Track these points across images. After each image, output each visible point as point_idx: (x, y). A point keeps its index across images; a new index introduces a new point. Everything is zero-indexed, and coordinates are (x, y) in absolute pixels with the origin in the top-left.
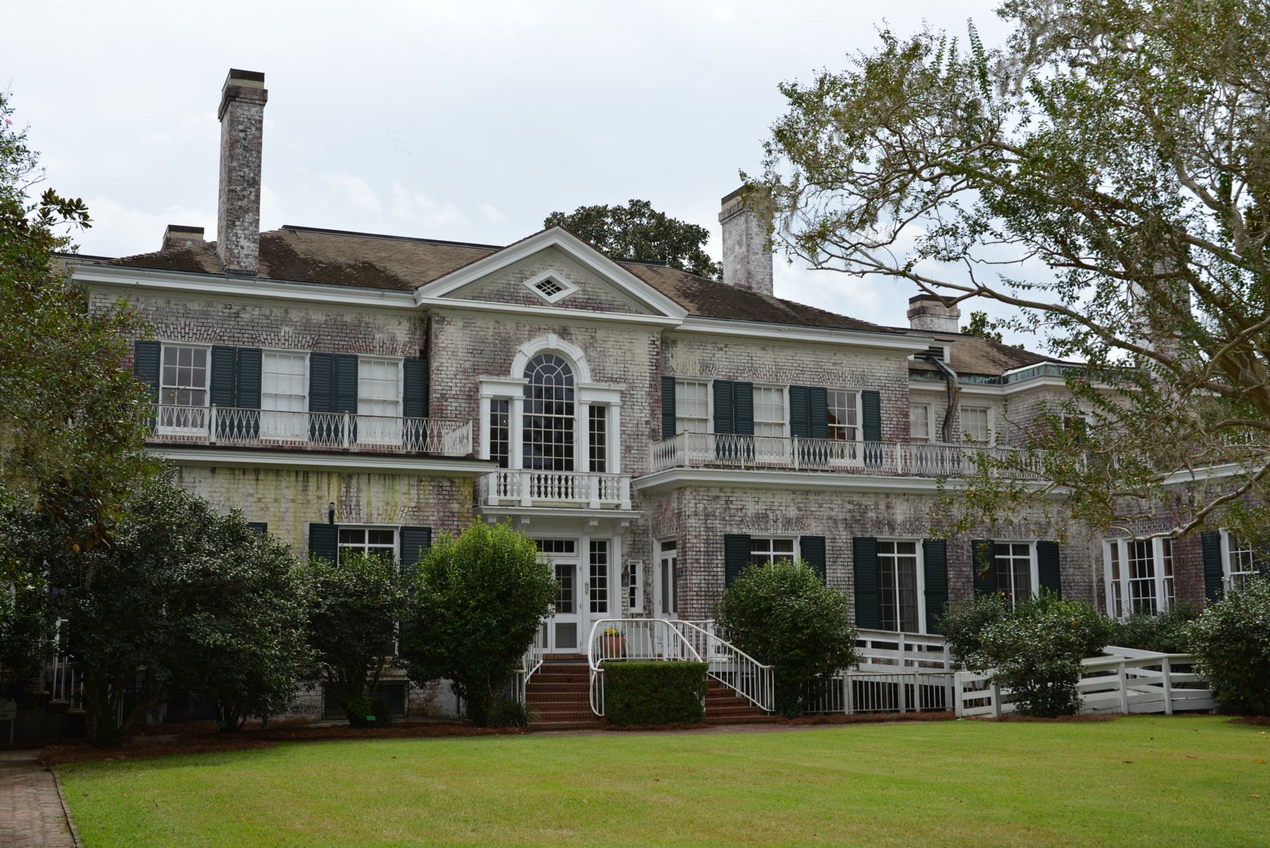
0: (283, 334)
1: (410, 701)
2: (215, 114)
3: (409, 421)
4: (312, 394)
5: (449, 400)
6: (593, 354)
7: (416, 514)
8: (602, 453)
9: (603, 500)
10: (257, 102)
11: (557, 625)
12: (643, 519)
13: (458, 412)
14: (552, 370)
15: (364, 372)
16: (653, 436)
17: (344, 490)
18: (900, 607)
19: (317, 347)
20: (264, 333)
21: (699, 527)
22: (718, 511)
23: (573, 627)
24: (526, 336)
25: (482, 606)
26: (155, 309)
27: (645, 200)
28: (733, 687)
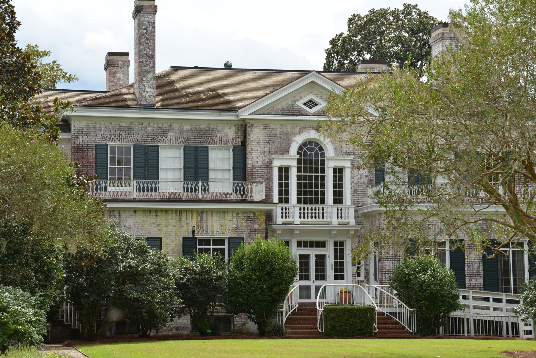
0: (169, 137)
1: (234, 325)
2: (131, 15)
4: (185, 167)
5: (256, 168)
7: (236, 231)
8: (341, 193)
10: (152, 13)
13: (261, 175)
17: (200, 219)
20: (160, 137)
24: (298, 132)
25: (259, 279)
26: (104, 127)
27: (414, 4)
28: (397, 320)
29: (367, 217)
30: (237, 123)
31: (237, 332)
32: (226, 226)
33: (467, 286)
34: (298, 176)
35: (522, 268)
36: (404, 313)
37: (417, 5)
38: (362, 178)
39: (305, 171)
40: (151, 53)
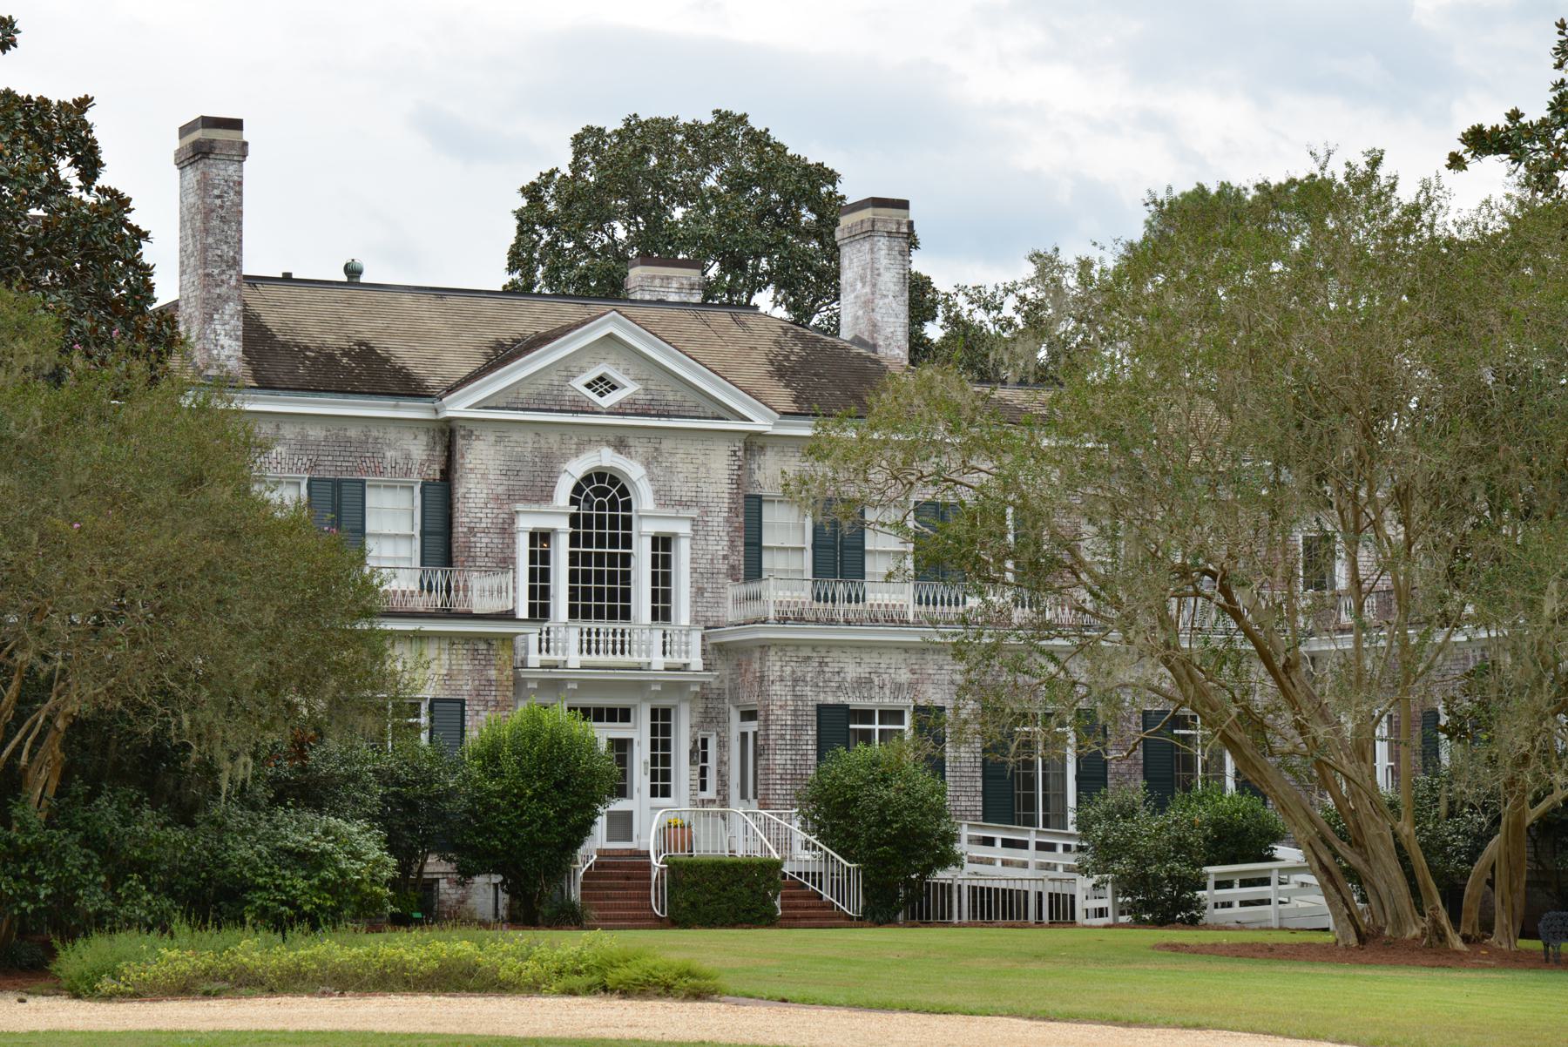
8: (666, 597)
9: (668, 659)
14: (605, 492)
15: (373, 499)
16: (732, 573)
18: (1044, 795)
23: (627, 816)
25: (539, 796)
27: (738, 112)
34: (571, 553)
36: (820, 874)
39: (588, 544)
40: (232, 254)
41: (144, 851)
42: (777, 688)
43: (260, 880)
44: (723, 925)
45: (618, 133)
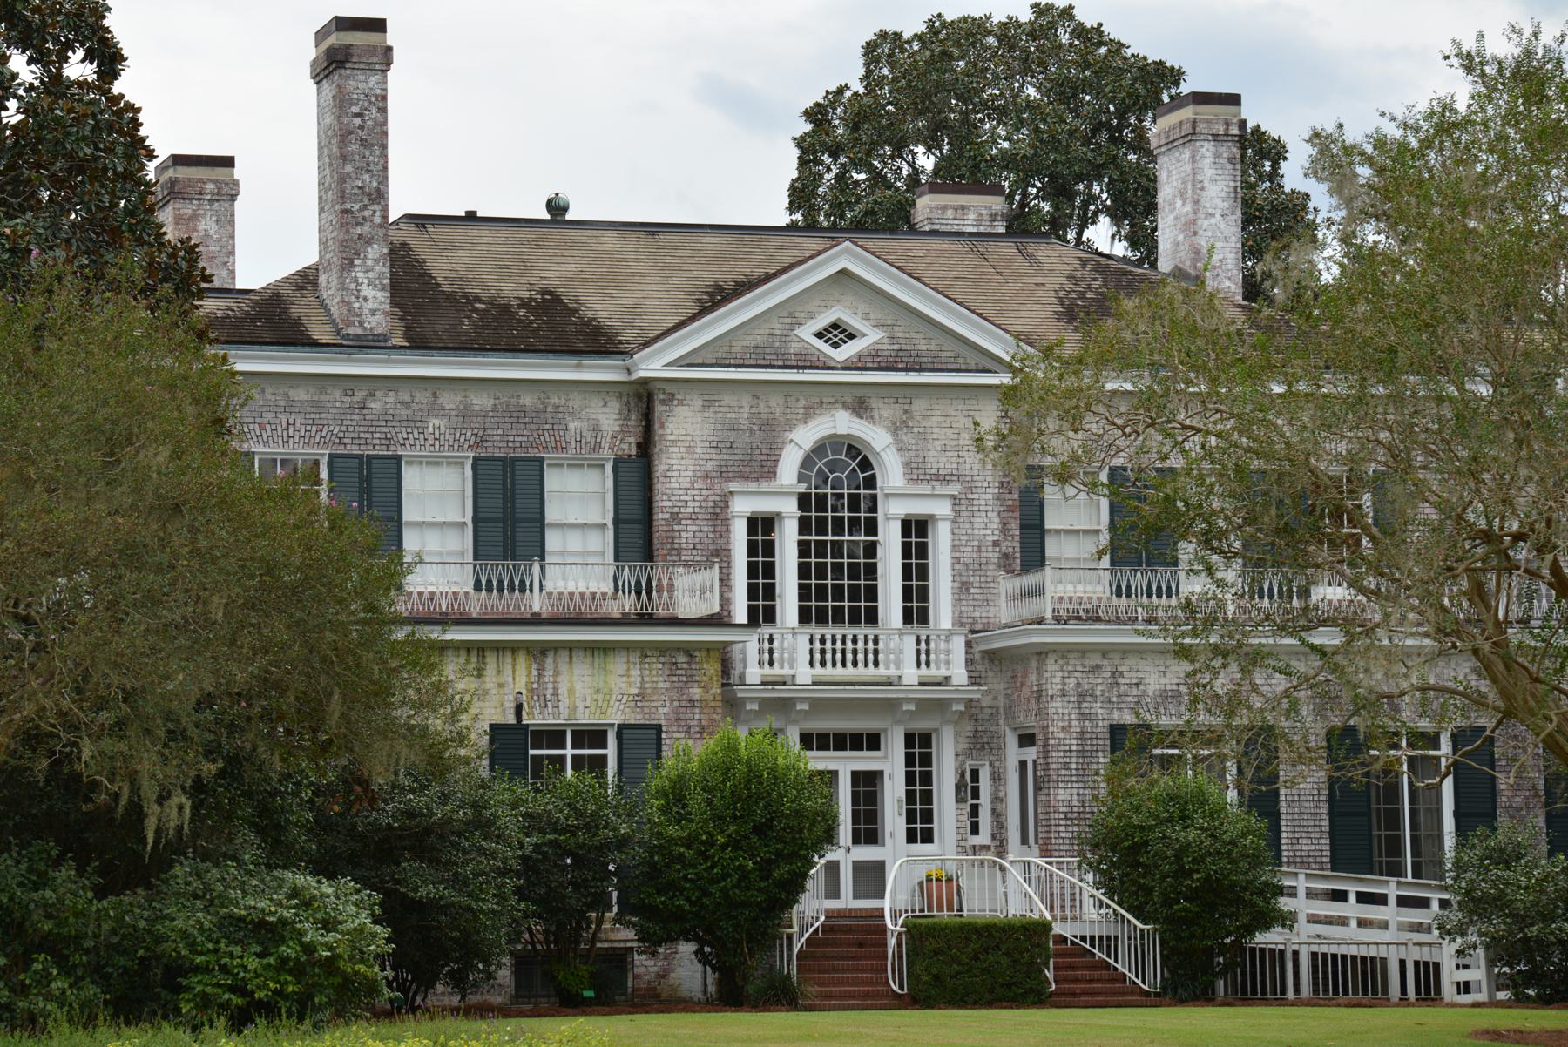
0: (431, 430)
1: (635, 977)
3: (626, 569)
5: (684, 522)
6: (907, 438)
8: (923, 594)
10: (378, 67)
11: (854, 863)
12: (990, 697)
13: (697, 540)
15: (554, 481)
16: (1006, 564)
17: (535, 673)
19: (482, 447)
20: (403, 430)
21: (1069, 714)
22: (1100, 688)
24: (800, 416)
25: (735, 843)
28: (1104, 957)
29: (996, 662)
30: (625, 389)
31: (644, 997)
32: (610, 693)
33: (1285, 860)
34: (800, 543)
35: (1434, 806)
36: (1116, 938)
37: (1100, 25)
38: (983, 549)
40: (375, 184)
41: (58, 925)
42: (1057, 705)
43: (199, 959)
44: (977, 1003)
45: (919, 37)
